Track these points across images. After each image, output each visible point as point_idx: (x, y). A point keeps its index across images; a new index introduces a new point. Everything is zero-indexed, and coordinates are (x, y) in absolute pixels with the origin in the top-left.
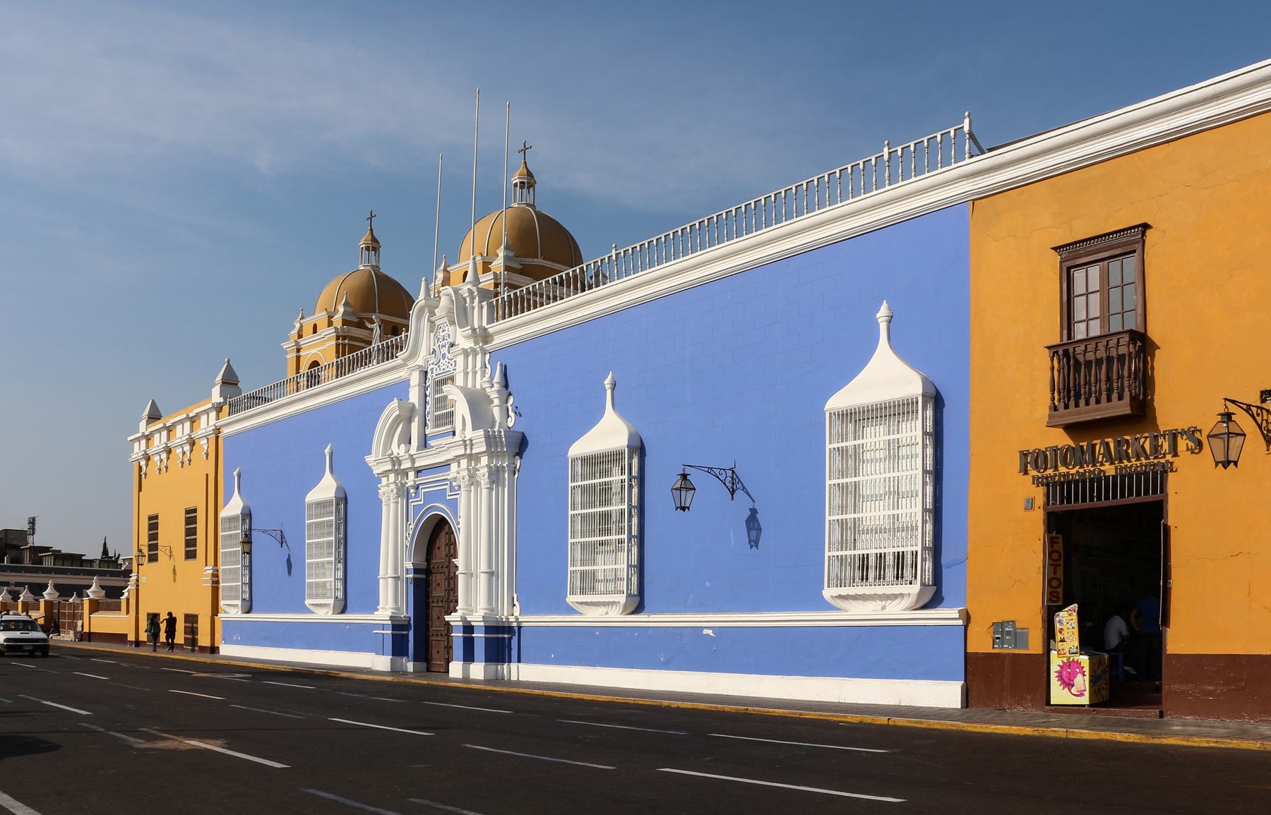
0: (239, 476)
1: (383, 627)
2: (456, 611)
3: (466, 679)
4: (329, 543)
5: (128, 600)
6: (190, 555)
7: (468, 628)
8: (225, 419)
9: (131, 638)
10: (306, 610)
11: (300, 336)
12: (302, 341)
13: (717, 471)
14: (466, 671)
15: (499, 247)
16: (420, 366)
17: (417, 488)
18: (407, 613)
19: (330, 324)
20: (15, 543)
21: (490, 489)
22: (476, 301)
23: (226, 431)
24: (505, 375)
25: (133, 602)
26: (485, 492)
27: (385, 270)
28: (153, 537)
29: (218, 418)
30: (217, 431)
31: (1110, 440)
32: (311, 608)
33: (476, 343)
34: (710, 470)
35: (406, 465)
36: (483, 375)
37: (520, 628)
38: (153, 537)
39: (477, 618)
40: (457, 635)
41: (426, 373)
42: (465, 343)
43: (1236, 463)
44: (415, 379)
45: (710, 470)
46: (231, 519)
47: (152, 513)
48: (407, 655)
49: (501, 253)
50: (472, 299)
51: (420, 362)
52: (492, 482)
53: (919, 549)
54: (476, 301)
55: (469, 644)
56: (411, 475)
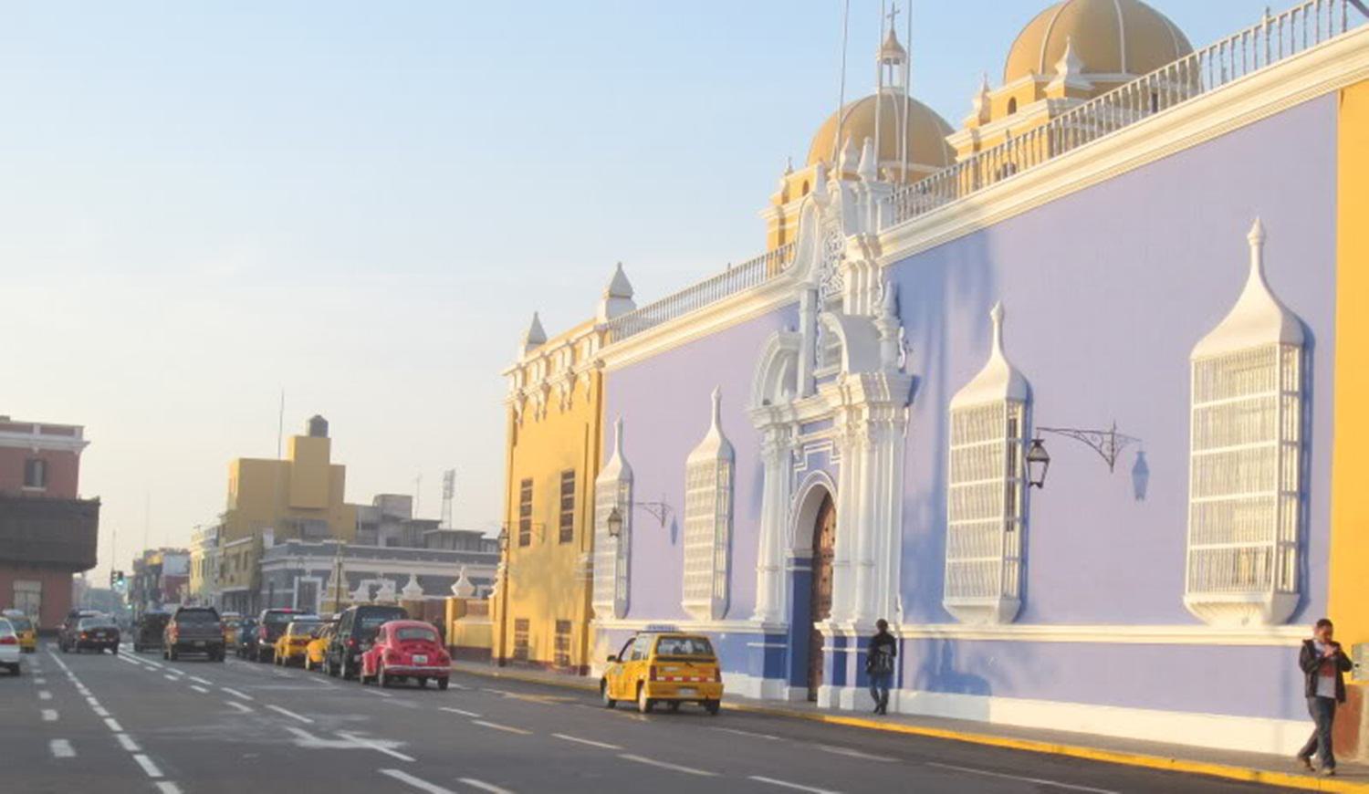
0: (621, 426)
1: (754, 637)
2: (828, 616)
3: (835, 710)
4: (709, 521)
5: (495, 598)
6: (566, 537)
7: (841, 641)
8: (609, 348)
9: (496, 653)
10: (1180, 615)
11: (785, 199)
12: (788, 209)
13: (1088, 436)
14: (835, 698)
15: (1059, 58)
16: (808, 284)
17: (801, 447)
18: (783, 619)
19: (1039, 94)
20: (395, 513)
21: (871, 451)
22: (869, 197)
23: (611, 364)
24: (897, 300)
25: (500, 602)
26: (864, 456)
27: (917, 93)
28: (567, 504)
29: (602, 344)
30: (601, 363)
31: (689, 492)
32: (955, 613)
33: (866, 254)
34: (1077, 434)
35: (788, 418)
36: (874, 299)
37: (902, 640)
38: (567, 504)
39: (849, 630)
40: (828, 649)
41: (816, 293)
42: (855, 255)
43: (1040, 485)
44: (804, 299)
45: (1077, 434)
46: (607, 487)
47: (526, 476)
48: (784, 677)
49: (1062, 68)
50: (865, 194)
51: (810, 279)
52: (873, 442)
53: (1273, 544)
54: (869, 197)
55: (840, 659)
56: (795, 430)
